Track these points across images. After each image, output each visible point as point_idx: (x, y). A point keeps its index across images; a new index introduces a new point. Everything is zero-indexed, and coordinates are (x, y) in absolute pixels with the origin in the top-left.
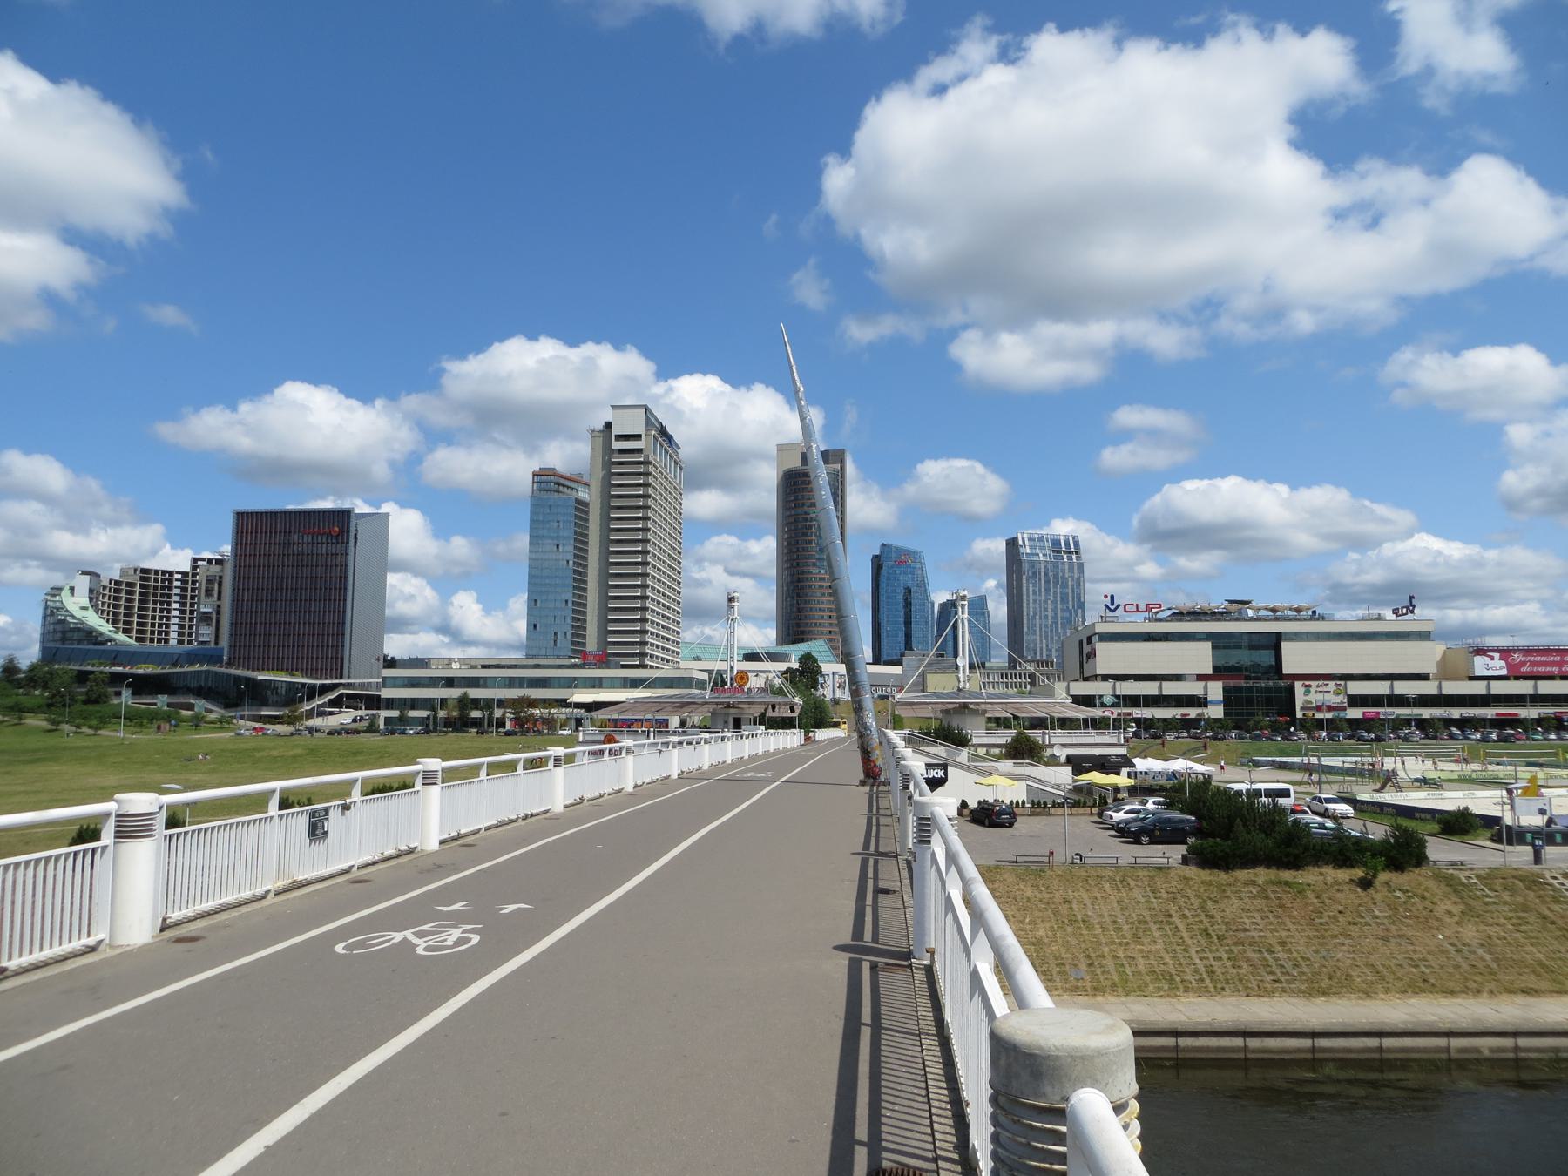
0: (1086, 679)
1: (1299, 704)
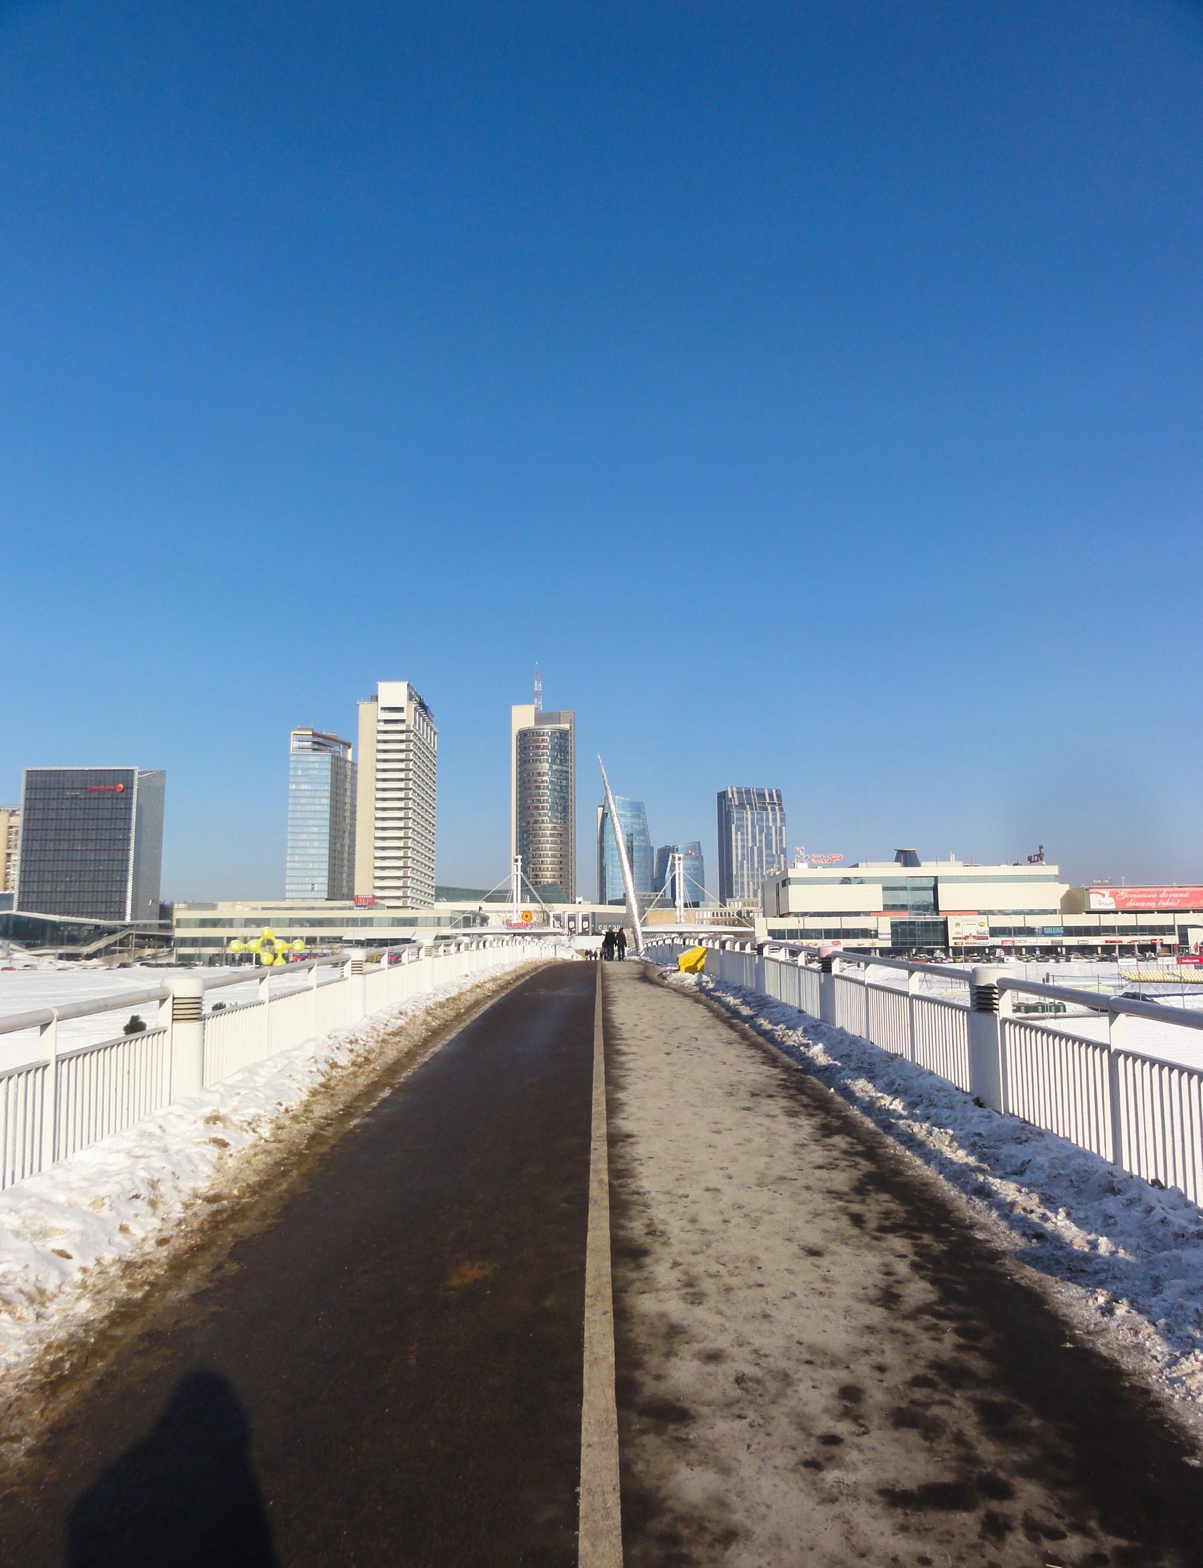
0: (782, 916)
1: (951, 935)
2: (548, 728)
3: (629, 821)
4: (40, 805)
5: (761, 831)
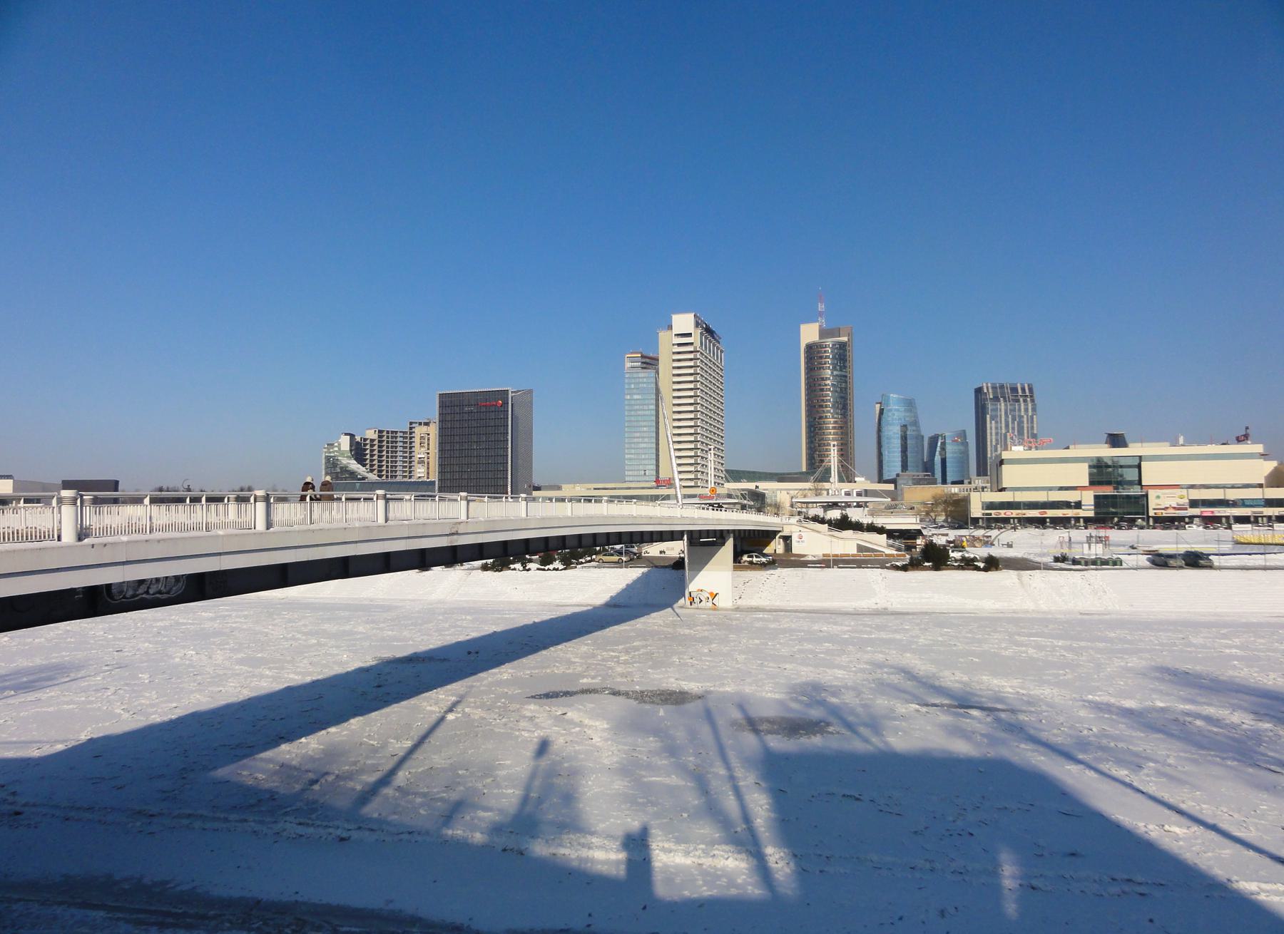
2: (829, 342)
3: (902, 414)
4: (449, 418)
5: (1014, 420)
